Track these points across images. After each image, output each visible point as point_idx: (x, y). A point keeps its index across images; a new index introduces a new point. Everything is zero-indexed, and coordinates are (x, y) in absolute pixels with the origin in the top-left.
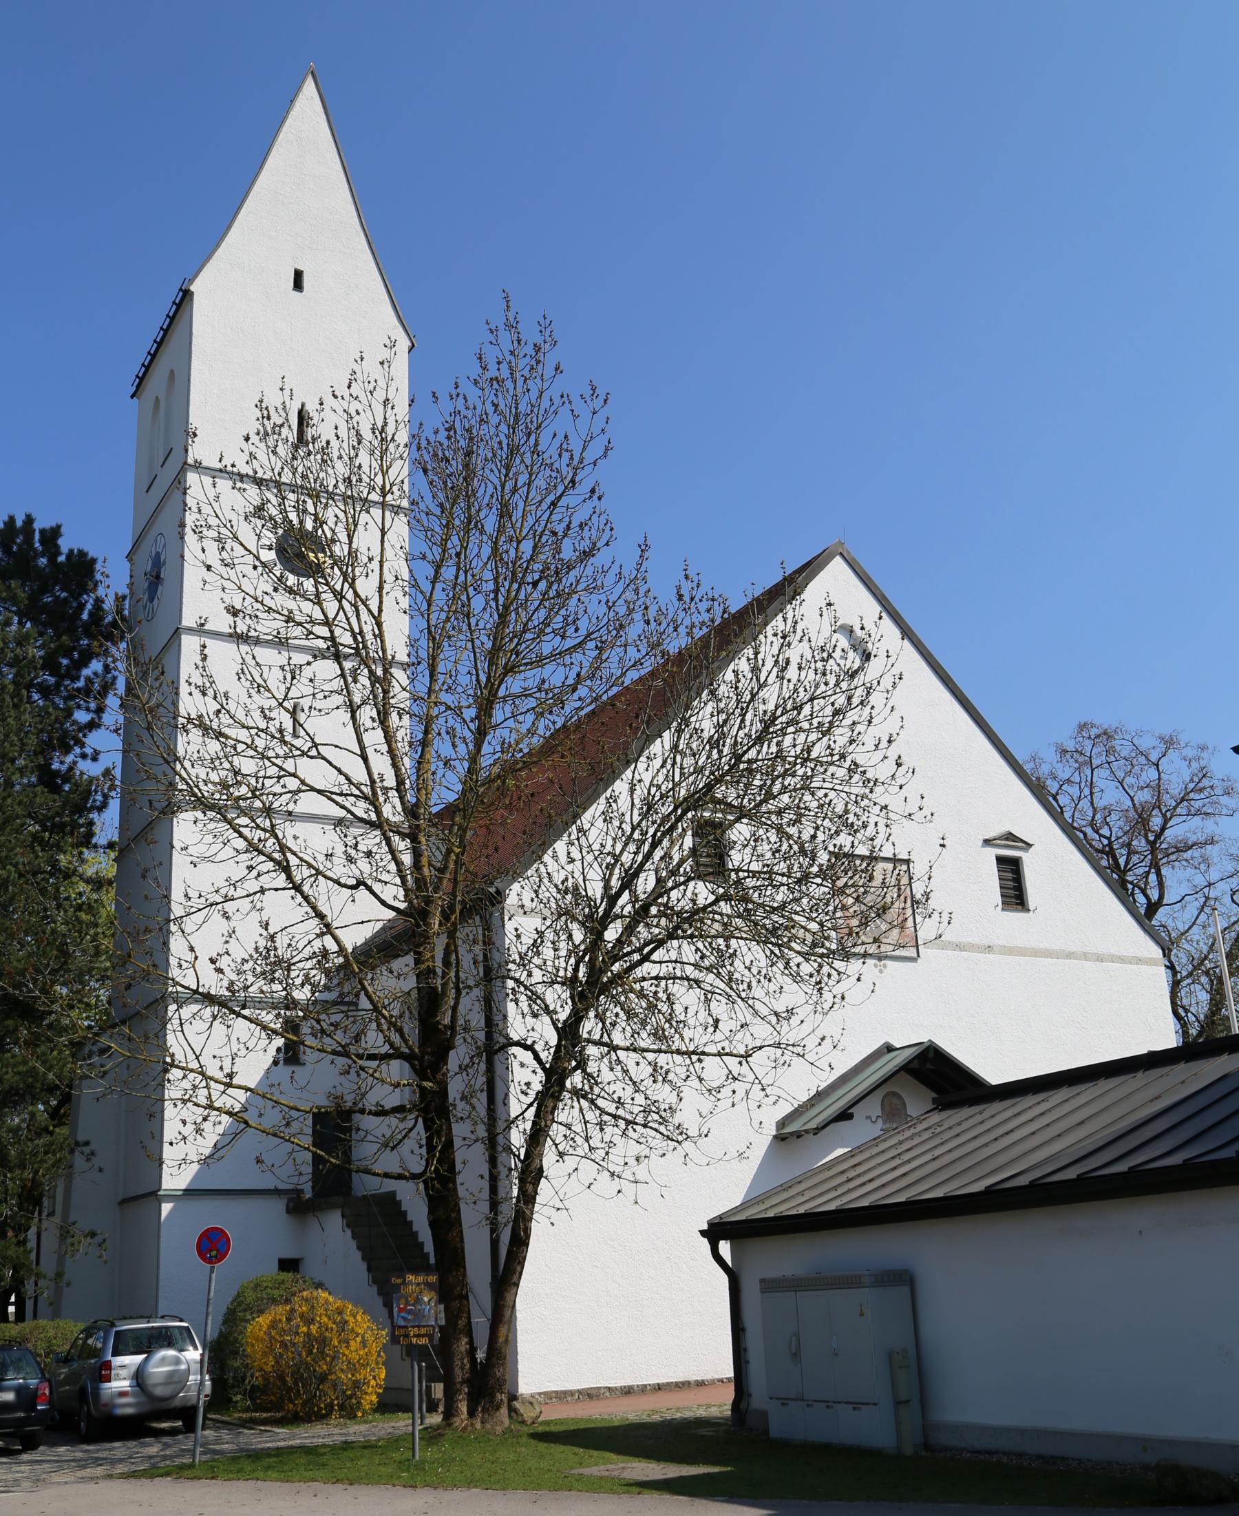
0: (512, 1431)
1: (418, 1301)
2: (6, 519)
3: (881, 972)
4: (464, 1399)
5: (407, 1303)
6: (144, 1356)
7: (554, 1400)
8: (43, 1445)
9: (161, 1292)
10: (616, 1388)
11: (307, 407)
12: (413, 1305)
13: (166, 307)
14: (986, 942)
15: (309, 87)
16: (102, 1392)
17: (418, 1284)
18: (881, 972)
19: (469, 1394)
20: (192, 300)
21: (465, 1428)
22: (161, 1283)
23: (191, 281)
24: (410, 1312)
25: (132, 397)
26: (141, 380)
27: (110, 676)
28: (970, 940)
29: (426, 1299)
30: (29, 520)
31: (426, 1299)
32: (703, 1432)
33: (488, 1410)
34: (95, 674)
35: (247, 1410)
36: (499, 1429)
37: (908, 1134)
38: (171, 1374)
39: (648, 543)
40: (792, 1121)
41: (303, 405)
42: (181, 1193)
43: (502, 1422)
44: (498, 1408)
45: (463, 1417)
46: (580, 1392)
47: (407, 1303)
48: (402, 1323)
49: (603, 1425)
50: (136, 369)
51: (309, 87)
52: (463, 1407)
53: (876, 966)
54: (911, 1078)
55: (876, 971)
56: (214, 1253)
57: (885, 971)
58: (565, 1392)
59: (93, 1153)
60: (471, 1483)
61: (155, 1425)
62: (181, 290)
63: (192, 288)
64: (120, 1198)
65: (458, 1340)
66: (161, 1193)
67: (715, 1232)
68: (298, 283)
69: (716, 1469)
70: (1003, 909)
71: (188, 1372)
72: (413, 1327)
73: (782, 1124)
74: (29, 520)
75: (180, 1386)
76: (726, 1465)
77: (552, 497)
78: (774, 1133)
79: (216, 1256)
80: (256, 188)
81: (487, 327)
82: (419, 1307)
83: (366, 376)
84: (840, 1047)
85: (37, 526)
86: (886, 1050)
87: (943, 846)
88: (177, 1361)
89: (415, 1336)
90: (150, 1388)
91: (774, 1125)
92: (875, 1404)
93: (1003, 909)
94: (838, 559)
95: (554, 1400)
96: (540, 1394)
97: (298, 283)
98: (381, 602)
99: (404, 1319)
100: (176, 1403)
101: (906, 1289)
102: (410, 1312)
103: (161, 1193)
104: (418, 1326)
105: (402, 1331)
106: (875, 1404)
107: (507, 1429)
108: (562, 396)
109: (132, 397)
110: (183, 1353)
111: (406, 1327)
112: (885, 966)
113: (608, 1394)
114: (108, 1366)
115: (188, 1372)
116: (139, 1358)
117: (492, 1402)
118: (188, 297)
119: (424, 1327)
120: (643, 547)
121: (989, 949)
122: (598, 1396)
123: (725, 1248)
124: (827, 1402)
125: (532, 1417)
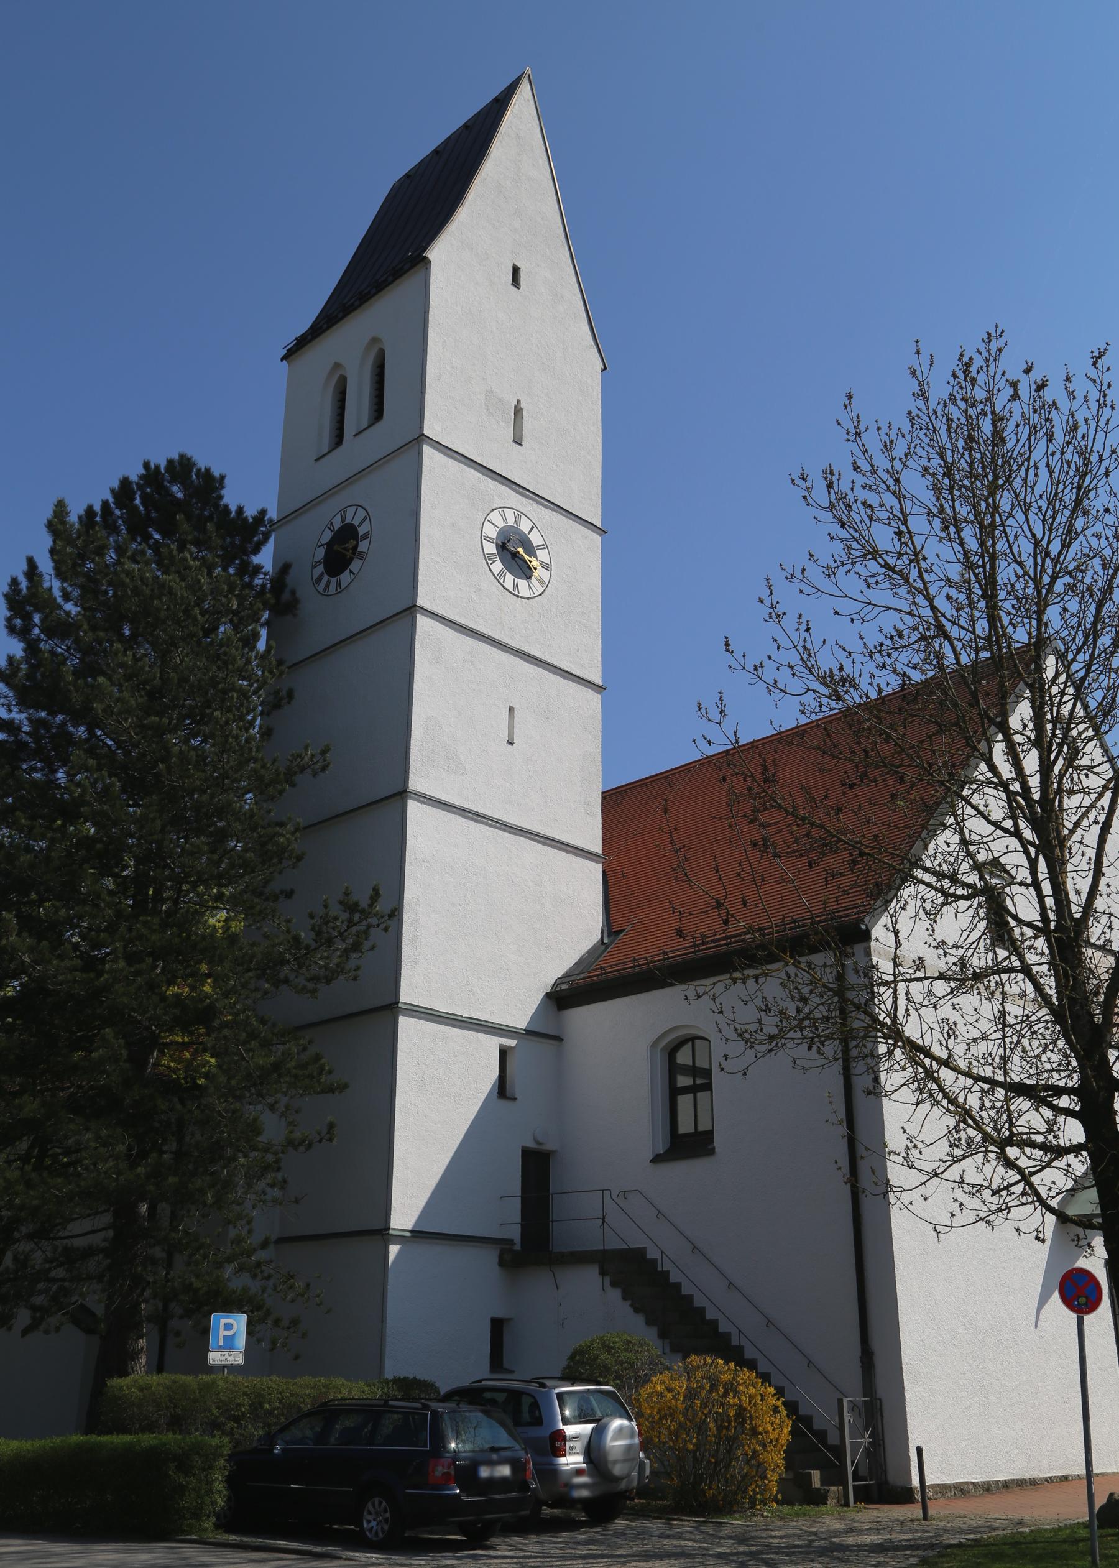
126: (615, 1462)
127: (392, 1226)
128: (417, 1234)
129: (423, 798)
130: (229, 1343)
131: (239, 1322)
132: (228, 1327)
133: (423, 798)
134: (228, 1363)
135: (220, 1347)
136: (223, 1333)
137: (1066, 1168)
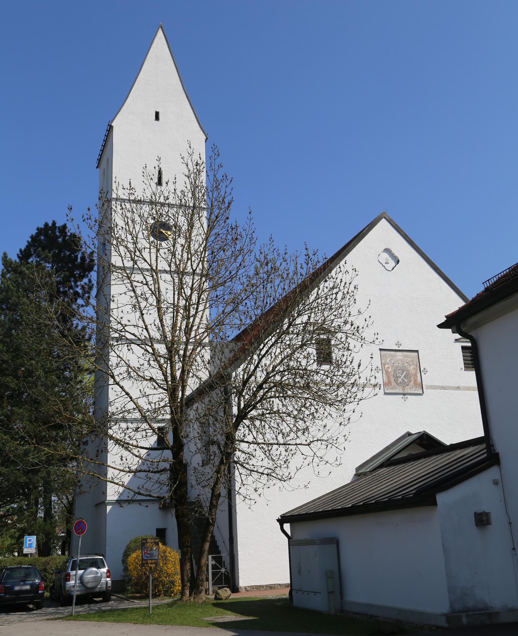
0: (206, 602)
1: (151, 549)
2: (44, 224)
3: (405, 400)
4: (188, 589)
5: (147, 551)
6: (83, 571)
7: (255, 589)
8: (45, 607)
9: (107, 543)
10: (283, 584)
11: (162, 169)
12: (150, 551)
13: (104, 132)
14: (457, 385)
15: (160, 33)
16: (66, 585)
17: (152, 543)
18: (405, 400)
19: (190, 587)
20: (113, 129)
21: (187, 601)
22: (107, 539)
23: (112, 121)
24: (148, 554)
25: (97, 168)
26: (99, 160)
27: (91, 284)
28: (449, 385)
29: (154, 549)
30: (54, 223)
31: (154, 549)
32: (278, 604)
33: (196, 593)
34: (85, 283)
35: (133, 593)
36: (200, 601)
37: (371, 476)
38: (95, 577)
39: (253, 237)
40: (363, 467)
41: (5, 254)
42: (115, 501)
43: (202, 598)
44: (200, 592)
45: (187, 596)
46: (266, 586)
47: (147, 551)
48: (145, 558)
49: (251, 600)
50: (97, 157)
51: (160, 33)
52: (187, 592)
53: (402, 398)
54: (420, 447)
55: (403, 400)
56: (80, 530)
57: (407, 400)
58: (260, 586)
59: (82, 485)
60: (182, 624)
61: (95, 599)
62: (108, 125)
63: (112, 124)
64: (96, 504)
65: (186, 564)
66: (106, 502)
67: (282, 520)
68: (157, 117)
69: (255, 618)
70: (465, 370)
71: (101, 577)
72: (150, 560)
73: (358, 469)
74: (54, 223)
75: (98, 583)
76: (248, 615)
77: (218, 219)
78: (355, 473)
79: (81, 532)
80: (138, 79)
81: (181, 156)
82: (152, 552)
83: (148, 174)
84: (348, 440)
85: (58, 225)
86: (408, 435)
87: (372, 358)
88: (97, 573)
89: (150, 563)
90: (85, 584)
91: (355, 469)
92: (320, 593)
93: (465, 370)
94: (383, 220)
95: (255, 589)
96: (248, 587)
97: (157, 117)
98: (157, 264)
99: (146, 556)
100: (97, 590)
101: (334, 546)
102: (148, 554)
103: (106, 502)
104: (151, 560)
105: (146, 562)
106: (320, 593)
107: (204, 601)
108: (223, 176)
109: (97, 168)
110: (99, 569)
111: (147, 560)
112: (407, 398)
113: (279, 587)
114: (69, 575)
115: (101, 577)
116: (82, 571)
117: (198, 590)
118: (111, 128)
119: (153, 560)
120: (251, 239)
121: (458, 388)
122: (274, 588)
123: (287, 527)
124: (308, 592)
125: (225, 597)
126: (88, 582)
127: (108, 499)
128: (119, 502)
129: (468, 389)
130: (30, 546)
131: (33, 539)
132: (30, 540)
133: (468, 389)
134: (30, 553)
135: (27, 547)
136: (28, 542)
137: (131, 350)
